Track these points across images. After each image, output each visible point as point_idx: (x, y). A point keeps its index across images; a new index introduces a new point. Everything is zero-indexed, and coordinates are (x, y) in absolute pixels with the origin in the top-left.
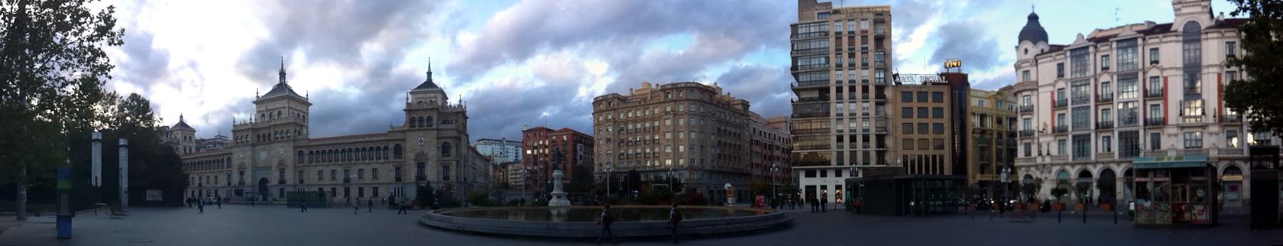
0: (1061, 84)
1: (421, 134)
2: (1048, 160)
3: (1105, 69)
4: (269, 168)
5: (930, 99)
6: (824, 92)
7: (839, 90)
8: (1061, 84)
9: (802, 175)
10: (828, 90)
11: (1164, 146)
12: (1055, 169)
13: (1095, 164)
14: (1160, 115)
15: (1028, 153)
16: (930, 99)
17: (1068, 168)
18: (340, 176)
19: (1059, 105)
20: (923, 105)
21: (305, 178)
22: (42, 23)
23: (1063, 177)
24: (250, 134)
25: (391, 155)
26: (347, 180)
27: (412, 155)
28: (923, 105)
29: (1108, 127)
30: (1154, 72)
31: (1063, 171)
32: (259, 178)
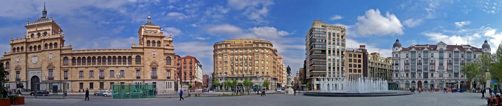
0: (407, 59)
1: (154, 50)
2: (403, 78)
3: (420, 57)
4: (40, 69)
5: (353, 56)
6: (324, 51)
7: (330, 52)
8: (407, 59)
9: (315, 80)
10: (325, 51)
11: (434, 76)
12: (405, 80)
13: (416, 80)
14: (451, 69)
15: (397, 76)
16: (353, 56)
17: (409, 81)
18: (97, 76)
19: (406, 64)
20: (355, 58)
21: (69, 76)
22: (426, 13)
23: (407, 82)
24: (24, 46)
25: (134, 61)
26: (102, 78)
27: (149, 63)
28: (355, 58)
29: (421, 71)
30: (432, 59)
31: (433, 81)
32: (31, 76)
